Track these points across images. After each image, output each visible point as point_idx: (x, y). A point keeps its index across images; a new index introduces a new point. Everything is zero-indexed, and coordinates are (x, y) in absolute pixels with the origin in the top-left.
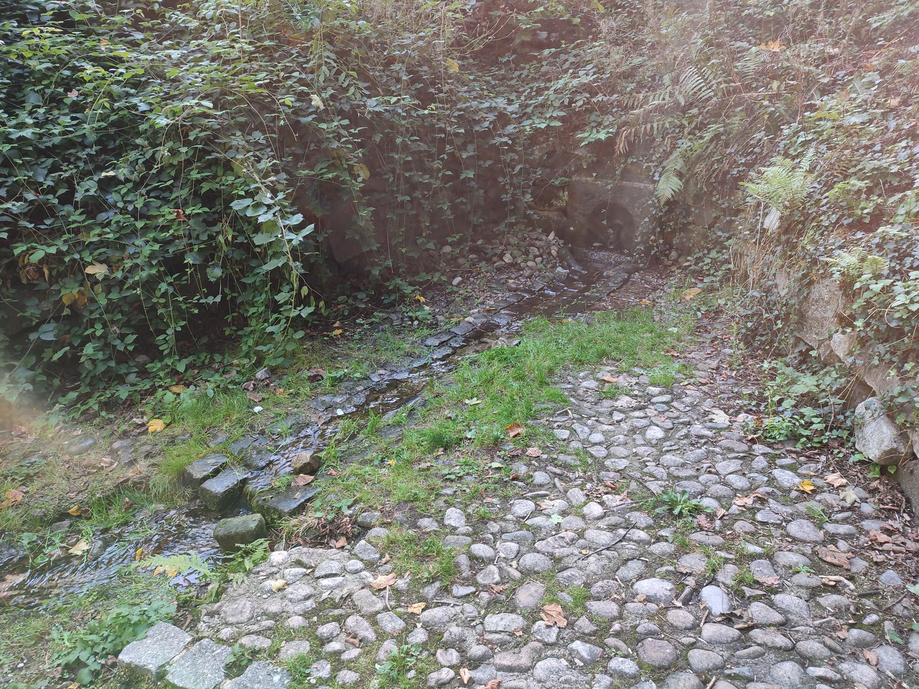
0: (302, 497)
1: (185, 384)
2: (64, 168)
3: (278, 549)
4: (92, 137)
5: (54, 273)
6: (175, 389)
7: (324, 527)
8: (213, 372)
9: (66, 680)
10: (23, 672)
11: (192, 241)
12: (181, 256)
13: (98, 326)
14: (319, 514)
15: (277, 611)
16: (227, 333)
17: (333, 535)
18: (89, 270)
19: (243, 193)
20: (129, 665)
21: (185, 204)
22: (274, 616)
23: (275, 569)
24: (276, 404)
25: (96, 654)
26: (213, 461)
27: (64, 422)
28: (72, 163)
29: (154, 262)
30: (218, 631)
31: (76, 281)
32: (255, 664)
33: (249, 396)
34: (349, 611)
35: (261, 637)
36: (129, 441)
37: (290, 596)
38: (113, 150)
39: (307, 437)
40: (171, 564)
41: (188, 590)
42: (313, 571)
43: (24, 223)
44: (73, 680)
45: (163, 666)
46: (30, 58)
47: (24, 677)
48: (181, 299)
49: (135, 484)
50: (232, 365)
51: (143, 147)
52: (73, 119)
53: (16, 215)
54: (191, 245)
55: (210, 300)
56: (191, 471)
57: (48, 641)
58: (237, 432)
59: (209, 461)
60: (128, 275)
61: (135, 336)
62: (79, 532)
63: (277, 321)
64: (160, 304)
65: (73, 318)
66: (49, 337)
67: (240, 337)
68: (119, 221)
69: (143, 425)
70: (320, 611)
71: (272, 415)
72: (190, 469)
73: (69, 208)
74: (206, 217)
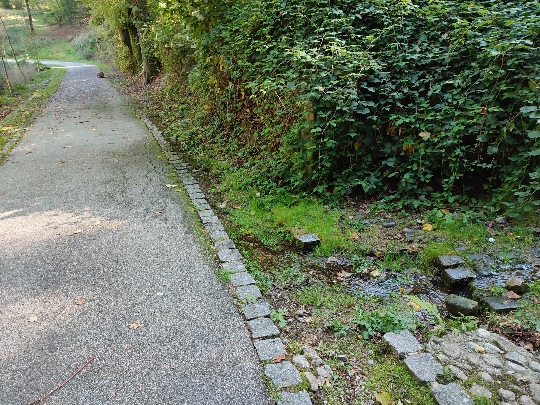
0: (508, 305)
1: (450, 210)
2: (427, 77)
3: (482, 328)
4: (448, 60)
5: (403, 133)
6: (443, 211)
7: (519, 330)
8: (468, 208)
9: (357, 332)
10: (340, 317)
11: (485, 128)
12: (474, 136)
13: (415, 165)
14: (517, 321)
15: (475, 363)
16: (485, 188)
17: (524, 339)
18: (421, 134)
19: (532, 102)
20: (387, 343)
21: (489, 104)
22: (473, 365)
23: (479, 339)
24: (505, 241)
25: (373, 328)
26: (455, 259)
27: (384, 209)
28: (431, 74)
29: (458, 136)
30: (437, 353)
31: (413, 139)
32: (454, 384)
33: (488, 230)
34: (524, 391)
35: (461, 371)
36: (412, 230)
37: (486, 360)
38: (456, 68)
39: (521, 269)
40: (419, 304)
41: (422, 322)
42: (505, 354)
43: (398, 104)
44: (360, 334)
45: (404, 353)
46: (428, 16)
47: (340, 320)
48: (466, 161)
49: (409, 253)
50: (482, 208)
51: (474, 68)
52: (440, 49)
53: (396, 99)
54: (483, 130)
55: (484, 165)
56: (441, 259)
57: (353, 309)
58: (475, 248)
59: (453, 259)
60: (441, 141)
61: (432, 175)
62: (377, 265)
63: (524, 190)
64: (452, 161)
65: (404, 159)
66: (391, 165)
67: (492, 192)
68: (446, 110)
69: (421, 224)
70: (504, 380)
71: (501, 247)
72: (441, 258)
73: (422, 99)
74: (499, 114)
